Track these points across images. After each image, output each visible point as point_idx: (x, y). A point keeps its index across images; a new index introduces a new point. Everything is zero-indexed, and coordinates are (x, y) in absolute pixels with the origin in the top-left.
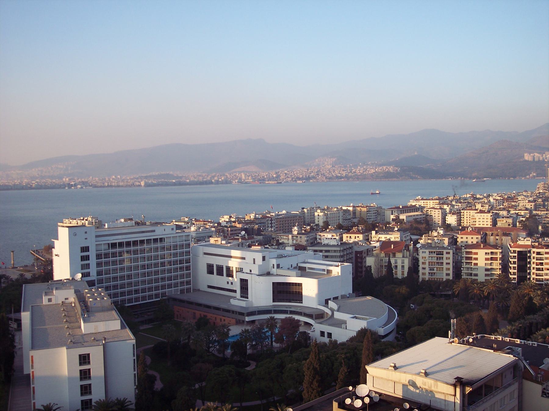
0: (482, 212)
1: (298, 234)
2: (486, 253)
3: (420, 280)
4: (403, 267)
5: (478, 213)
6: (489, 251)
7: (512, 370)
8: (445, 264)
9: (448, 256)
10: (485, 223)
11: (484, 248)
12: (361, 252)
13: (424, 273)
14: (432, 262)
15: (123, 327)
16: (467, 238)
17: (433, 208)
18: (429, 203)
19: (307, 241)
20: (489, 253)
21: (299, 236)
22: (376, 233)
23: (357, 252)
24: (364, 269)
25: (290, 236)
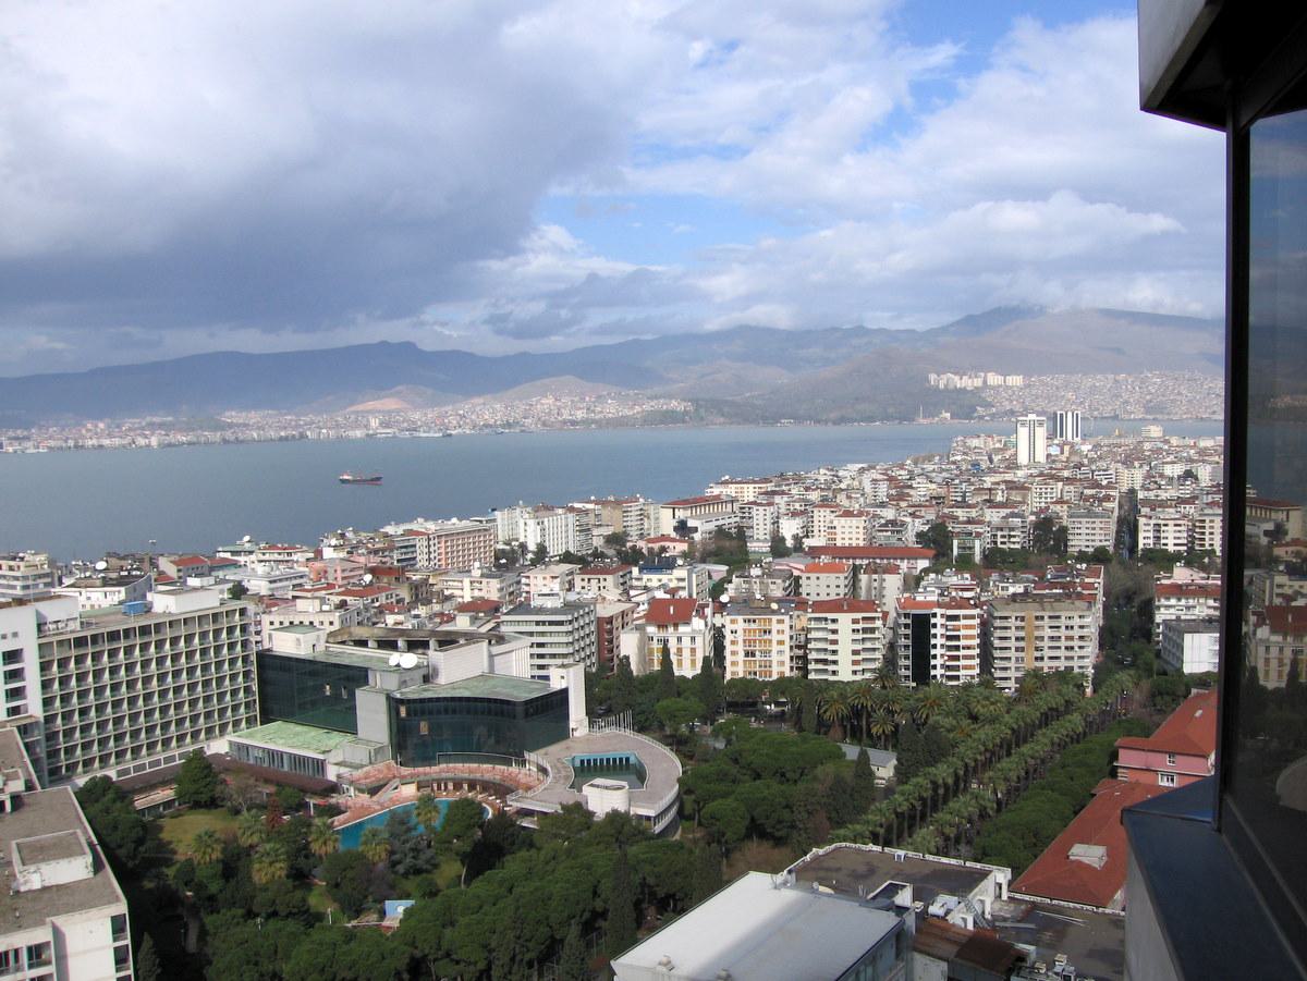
0: (848, 514)
1: (482, 576)
2: (854, 631)
3: (728, 676)
4: (693, 651)
5: (841, 516)
6: (859, 616)
7: (894, 939)
8: (774, 643)
9: (780, 627)
10: (854, 536)
11: (851, 610)
12: (610, 620)
13: (736, 667)
14: (750, 640)
15: (97, 867)
16: (818, 578)
17: (755, 503)
18: (746, 490)
19: (501, 590)
20: (858, 631)
21: (484, 580)
22: (640, 571)
23: (600, 620)
24: (616, 661)
25: (467, 581)
